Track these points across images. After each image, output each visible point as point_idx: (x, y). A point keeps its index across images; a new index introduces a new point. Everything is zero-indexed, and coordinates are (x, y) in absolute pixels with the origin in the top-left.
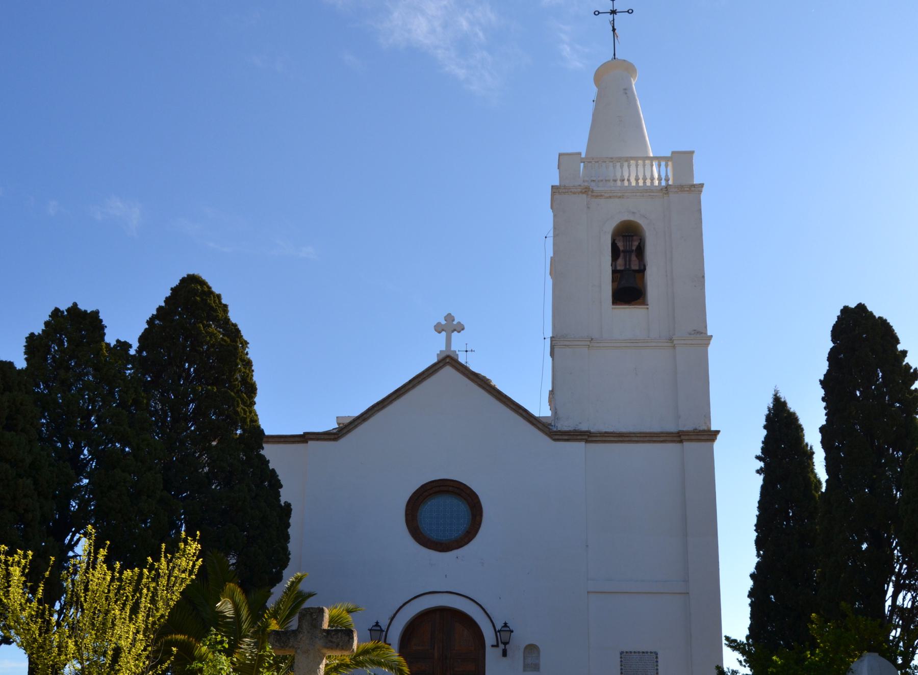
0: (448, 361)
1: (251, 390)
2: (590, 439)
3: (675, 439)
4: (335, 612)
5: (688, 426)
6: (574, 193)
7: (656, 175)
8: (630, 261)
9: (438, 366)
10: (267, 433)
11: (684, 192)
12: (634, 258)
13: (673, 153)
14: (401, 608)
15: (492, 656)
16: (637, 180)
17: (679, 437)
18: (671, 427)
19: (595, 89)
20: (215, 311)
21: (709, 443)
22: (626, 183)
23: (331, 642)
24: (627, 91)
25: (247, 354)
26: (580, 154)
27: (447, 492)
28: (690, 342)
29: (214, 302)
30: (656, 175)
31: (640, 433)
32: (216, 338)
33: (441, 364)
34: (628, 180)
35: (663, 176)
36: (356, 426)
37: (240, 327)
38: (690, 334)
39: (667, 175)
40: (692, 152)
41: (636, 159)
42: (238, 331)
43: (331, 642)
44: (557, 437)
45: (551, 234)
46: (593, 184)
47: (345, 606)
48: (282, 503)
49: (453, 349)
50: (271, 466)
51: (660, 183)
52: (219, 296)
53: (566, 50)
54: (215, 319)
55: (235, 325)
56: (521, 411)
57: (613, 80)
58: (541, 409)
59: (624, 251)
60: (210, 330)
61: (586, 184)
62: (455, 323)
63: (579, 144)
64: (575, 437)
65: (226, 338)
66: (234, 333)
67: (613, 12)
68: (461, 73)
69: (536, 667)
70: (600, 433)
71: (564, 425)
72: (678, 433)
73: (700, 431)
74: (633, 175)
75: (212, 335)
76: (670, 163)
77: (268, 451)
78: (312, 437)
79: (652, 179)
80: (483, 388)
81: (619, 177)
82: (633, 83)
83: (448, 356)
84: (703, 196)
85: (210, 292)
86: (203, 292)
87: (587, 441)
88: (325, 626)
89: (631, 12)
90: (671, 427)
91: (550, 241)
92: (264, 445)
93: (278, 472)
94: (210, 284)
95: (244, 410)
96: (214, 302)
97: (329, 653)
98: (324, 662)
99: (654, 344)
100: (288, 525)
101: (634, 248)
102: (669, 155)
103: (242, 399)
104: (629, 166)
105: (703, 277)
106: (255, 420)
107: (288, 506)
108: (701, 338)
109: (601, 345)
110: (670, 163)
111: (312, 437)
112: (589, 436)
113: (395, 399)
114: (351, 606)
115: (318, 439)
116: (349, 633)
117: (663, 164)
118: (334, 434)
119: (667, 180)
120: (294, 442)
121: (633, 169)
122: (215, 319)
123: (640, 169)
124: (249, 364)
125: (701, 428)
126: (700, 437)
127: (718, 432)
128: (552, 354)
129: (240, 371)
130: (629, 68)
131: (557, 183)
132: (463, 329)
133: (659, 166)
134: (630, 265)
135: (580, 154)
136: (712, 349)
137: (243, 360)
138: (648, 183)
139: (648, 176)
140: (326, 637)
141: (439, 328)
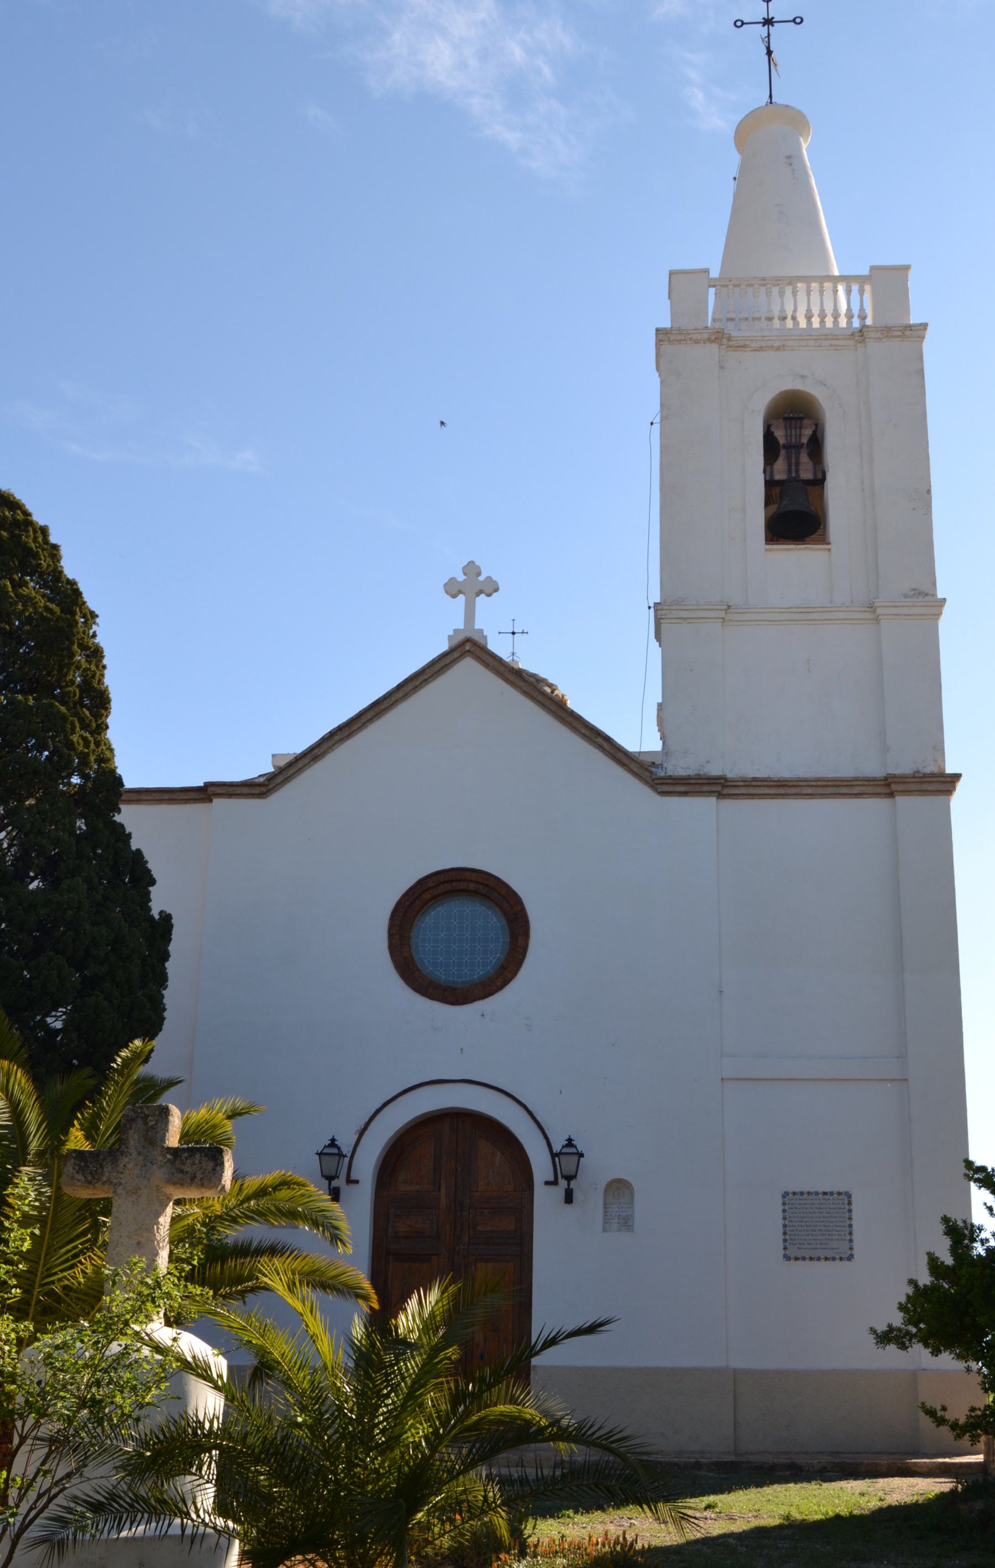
0: (469, 648)
1: (101, 702)
2: (726, 791)
3: (880, 790)
4: (200, 1114)
5: (905, 767)
6: (697, 342)
7: (843, 307)
8: (797, 464)
9: (450, 658)
10: (129, 783)
11: (893, 338)
12: (804, 458)
13: (873, 268)
14: (378, 1112)
15: (545, 1200)
16: (809, 317)
17: (888, 786)
18: (872, 767)
19: (736, 158)
20: (36, 556)
21: (940, 799)
22: (789, 324)
23: (182, 1171)
24: (793, 160)
25: (94, 635)
26: (706, 271)
27: (475, 894)
28: (906, 611)
29: (35, 540)
30: (843, 307)
31: (817, 780)
32: (35, 605)
33: (456, 655)
34: (794, 318)
35: (856, 311)
36: (300, 771)
37: (82, 587)
38: (906, 596)
39: (862, 309)
40: (907, 268)
41: (807, 280)
42: (78, 593)
43: (182, 1171)
44: (665, 788)
45: (658, 420)
46: (731, 325)
47: (228, 1107)
48: (155, 913)
49: (477, 627)
50: (134, 845)
51: (849, 322)
52: (44, 531)
53: (697, 97)
54: (35, 570)
55: (72, 583)
56: (600, 740)
57: (768, 140)
58: (641, 737)
59: (785, 447)
60: (24, 591)
61: (718, 325)
62: (481, 578)
63: (712, 260)
64: (698, 788)
65: (53, 606)
66: (70, 596)
67: (768, 22)
68: (512, 139)
69: (626, 1224)
70: (744, 780)
71: (679, 767)
72: (886, 779)
73: (925, 775)
74: (802, 309)
75: (27, 600)
76: (867, 288)
77: (128, 816)
78: (219, 790)
79: (836, 316)
80: (532, 698)
81: (776, 313)
82: (804, 147)
83: (468, 640)
84: (927, 346)
85: (26, 522)
86: (16, 523)
87: (720, 796)
88: (173, 1140)
89: (798, 21)
90: (873, 769)
91: (657, 427)
92: (122, 807)
93: (147, 855)
94: (29, 507)
95: (85, 739)
96: (35, 540)
97: (178, 1194)
98: (169, 1210)
99: (842, 615)
100: (166, 956)
101: (805, 440)
102: (866, 272)
103: (82, 720)
104: (794, 293)
105: (929, 492)
106: (106, 758)
107: (166, 919)
108: (925, 603)
109: (746, 617)
110: (867, 288)
111: (219, 790)
112: (724, 786)
113: (371, 720)
114: (240, 1104)
115: (230, 795)
116: (216, 1156)
117: (855, 288)
118: (260, 785)
119: (863, 317)
120: (186, 801)
121: (802, 297)
122: (35, 570)
123: (815, 297)
124: (96, 654)
125: (927, 771)
126: (924, 787)
127: (957, 777)
128: (658, 637)
129: (78, 668)
130: (796, 121)
131: (667, 324)
132: (496, 590)
133: (848, 292)
134: (797, 471)
135: (706, 271)
136: (945, 624)
137: (83, 647)
138: (829, 323)
139: (829, 310)
140: (172, 1162)
141: (453, 589)
